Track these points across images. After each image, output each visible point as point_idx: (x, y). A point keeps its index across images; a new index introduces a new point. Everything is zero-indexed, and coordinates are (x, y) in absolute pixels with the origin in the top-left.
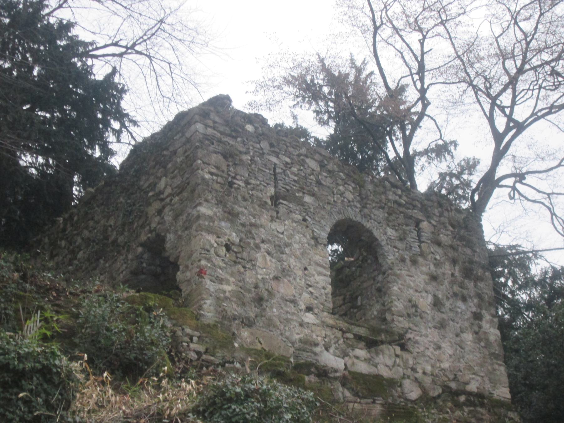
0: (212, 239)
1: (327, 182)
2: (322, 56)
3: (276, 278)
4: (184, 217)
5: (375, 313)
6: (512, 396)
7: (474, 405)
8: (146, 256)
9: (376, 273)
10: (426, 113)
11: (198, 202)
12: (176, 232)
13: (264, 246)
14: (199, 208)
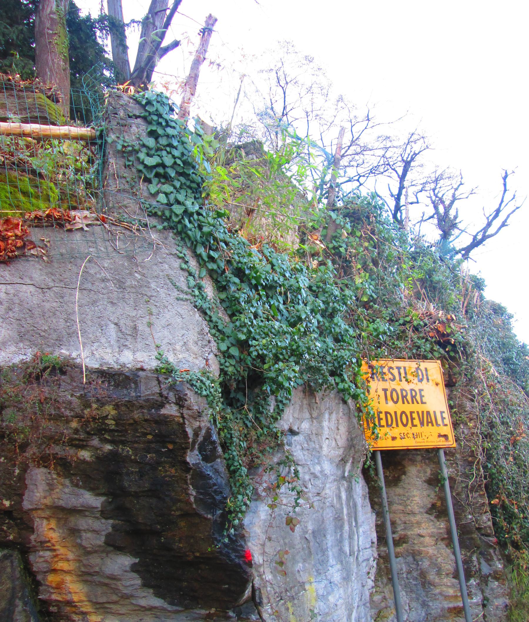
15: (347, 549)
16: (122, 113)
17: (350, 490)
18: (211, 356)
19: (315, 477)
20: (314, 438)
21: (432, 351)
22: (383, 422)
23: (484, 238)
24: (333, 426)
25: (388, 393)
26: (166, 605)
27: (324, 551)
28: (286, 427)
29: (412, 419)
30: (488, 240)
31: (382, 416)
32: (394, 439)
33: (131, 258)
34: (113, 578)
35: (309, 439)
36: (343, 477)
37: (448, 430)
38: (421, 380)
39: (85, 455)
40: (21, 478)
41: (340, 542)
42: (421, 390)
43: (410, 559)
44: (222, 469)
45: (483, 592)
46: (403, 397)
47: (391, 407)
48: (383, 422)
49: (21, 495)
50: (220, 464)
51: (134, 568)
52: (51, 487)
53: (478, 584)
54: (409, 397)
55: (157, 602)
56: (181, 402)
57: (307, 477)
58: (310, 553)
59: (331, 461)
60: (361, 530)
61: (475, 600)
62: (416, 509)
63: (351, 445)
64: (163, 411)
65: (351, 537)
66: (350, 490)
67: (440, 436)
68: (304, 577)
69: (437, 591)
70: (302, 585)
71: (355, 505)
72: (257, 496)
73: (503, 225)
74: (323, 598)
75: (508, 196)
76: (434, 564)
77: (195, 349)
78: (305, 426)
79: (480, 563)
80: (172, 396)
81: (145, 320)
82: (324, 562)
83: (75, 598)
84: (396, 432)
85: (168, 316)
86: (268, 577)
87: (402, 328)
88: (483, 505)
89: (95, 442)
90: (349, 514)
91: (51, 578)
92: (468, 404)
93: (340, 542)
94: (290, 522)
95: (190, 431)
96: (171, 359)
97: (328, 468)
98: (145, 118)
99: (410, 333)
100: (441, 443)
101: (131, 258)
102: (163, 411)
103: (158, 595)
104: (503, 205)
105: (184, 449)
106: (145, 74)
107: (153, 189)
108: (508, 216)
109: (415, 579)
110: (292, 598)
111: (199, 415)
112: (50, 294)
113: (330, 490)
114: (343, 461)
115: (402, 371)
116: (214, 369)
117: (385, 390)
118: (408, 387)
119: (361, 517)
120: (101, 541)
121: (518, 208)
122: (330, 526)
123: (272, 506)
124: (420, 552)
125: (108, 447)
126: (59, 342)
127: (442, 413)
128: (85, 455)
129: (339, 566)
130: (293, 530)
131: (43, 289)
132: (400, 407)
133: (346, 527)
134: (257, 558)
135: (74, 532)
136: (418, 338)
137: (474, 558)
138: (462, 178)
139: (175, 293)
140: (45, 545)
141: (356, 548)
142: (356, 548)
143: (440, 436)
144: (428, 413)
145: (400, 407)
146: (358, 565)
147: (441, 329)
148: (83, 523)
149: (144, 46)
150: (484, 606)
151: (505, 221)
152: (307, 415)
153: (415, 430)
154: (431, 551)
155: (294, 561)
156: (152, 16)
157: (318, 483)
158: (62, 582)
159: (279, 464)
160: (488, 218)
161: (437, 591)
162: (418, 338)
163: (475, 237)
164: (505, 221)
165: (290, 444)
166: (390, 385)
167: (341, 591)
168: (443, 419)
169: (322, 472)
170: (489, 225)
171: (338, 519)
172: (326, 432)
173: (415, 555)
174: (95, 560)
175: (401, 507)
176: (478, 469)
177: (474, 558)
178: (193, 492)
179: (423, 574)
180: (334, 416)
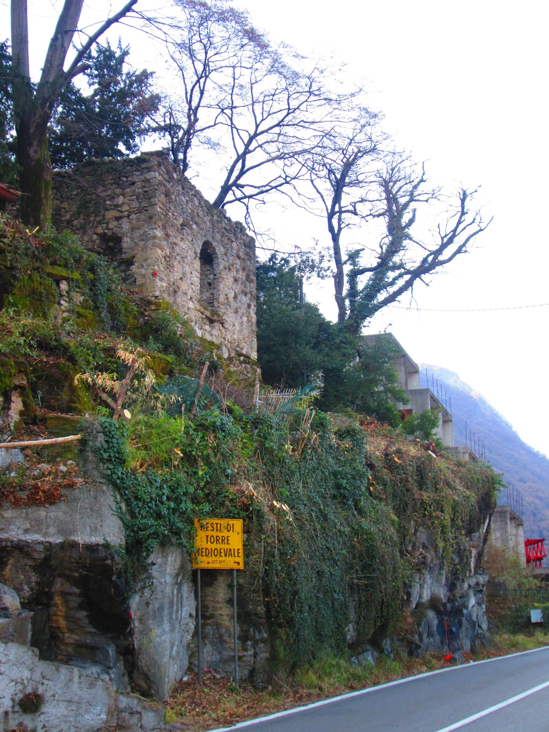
0: (159, 251)
1: (201, 213)
2: (154, 75)
3: (181, 279)
4: (141, 232)
5: (205, 298)
6: (258, 357)
7: (246, 363)
8: (97, 242)
9: (208, 272)
10: (97, 40)
11: (154, 226)
12: (132, 239)
13: (178, 258)
14: (155, 231)
15: (174, 617)
16: (95, 432)
17: (179, 590)
18: (123, 537)
19: (162, 584)
20: (163, 566)
21: (238, 514)
22: (204, 554)
23: (435, 264)
24: (173, 559)
25: (209, 538)
26: (97, 631)
27: (162, 617)
28: (150, 562)
29: (221, 552)
30: (438, 268)
31: (204, 550)
32: (208, 563)
33: (95, 498)
34: (79, 619)
35: (160, 566)
36: (177, 583)
37: (241, 560)
38: (228, 531)
39: (76, 574)
40: (53, 581)
41: (171, 613)
42: (228, 537)
43: (215, 627)
44: (123, 582)
45: (255, 649)
46: (217, 540)
47: (210, 546)
48: (204, 554)
49: (51, 587)
50: (123, 579)
51: (87, 616)
52: (62, 585)
53: (252, 645)
54: (220, 541)
55: (93, 630)
56: (113, 559)
57: (158, 584)
58: (155, 617)
59: (171, 576)
60: (184, 609)
61: (249, 653)
62: (220, 600)
63: (182, 567)
64: (106, 562)
65: (177, 611)
66: (179, 590)
67: (235, 562)
68: (152, 626)
69: (228, 646)
70: (151, 630)
71: (182, 597)
72: (135, 592)
73: (459, 251)
74: (160, 636)
75: (468, 219)
76: (228, 631)
77: (117, 535)
78: (159, 560)
79: (254, 633)
80: (109, 557)
81: (100, 524)
82: (162, 621)
83: (62, 626)
84: (210, 559)
85: (108, 522)
86: (137, 624)
87: (223, 499)
88: (259, 601)
89: (81, 570)
90: (177, 602)
91: (54, 618)
92: (256, 545)
93: (171, 613)
94: (147, 604)
95: (114, 569)
96: (108, 540)
97: (168, 579)
98: (104, 433)
99: (227, 503)
100: (236, 566)
101: (95, 498)
102: (106, 562)
103: (94, 627)
104: (461, 227)
105: (112, 574)
106: (48, 104)
107: (105, 466)
108: (468, 240)
109: (216, 638)
110: (146, 634)
111: (118, 564)
112: (67, 515)
113: (168, 590)
114: (177, 575)
115: (219, 526)
116: (123, 543)
117: (207, 536)
118: (220, 535)
119: (185, 602)
120: (76, 605)
121: (481, 230)
122: (167, 606)
123: (140, 597)
124: (220, 624)
125: (85, 573)
126: (71, 534)
127: (238, 550)
128: (76, 574)
129: (169, 624)
130: (148, 607)
131: (65, 513)
132: (214, 546)
133: (175, 607)
134: (133, 616)
135: (67, 601)
136: (232, 506)
137: (251, 630)
138: (424, 174)
139: (111, 512)
140: (56, 605)
141: (179, 617)
142: (179, 617)
143: (235, 562)
144: (230, 550)
145: (214, 546)
146: (180, 625)
147: (245, 502)
148: (70, 598)
149: (49, 71)
150: (255, 657)
151: (464, 245)
152: (161, 555)
153: (221, 559)
154: (227, 623)
155: (148, 620)
156: (62, 36)
157: (163, 587)
158: (58, 620)
159: (145, 578)
160: (442, 239)
161: (228, 646)
162: (232, 506)
163: (425, 260)
164: (464, 245)
165: (151, 569)
166: (210, 533)
167: (169, 635)
168: (238, 553)
169: (165, 581)
170: (443, 246)
171: (171, 604)
172: (169, 562)
173: (218, 625)
174: (72, 613)
175: (212, 598)
176: (258, 581)
177: (251, 630)
178: (113, 590)
179: (221, 636)
180: (174, 555)
